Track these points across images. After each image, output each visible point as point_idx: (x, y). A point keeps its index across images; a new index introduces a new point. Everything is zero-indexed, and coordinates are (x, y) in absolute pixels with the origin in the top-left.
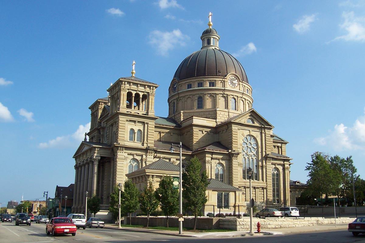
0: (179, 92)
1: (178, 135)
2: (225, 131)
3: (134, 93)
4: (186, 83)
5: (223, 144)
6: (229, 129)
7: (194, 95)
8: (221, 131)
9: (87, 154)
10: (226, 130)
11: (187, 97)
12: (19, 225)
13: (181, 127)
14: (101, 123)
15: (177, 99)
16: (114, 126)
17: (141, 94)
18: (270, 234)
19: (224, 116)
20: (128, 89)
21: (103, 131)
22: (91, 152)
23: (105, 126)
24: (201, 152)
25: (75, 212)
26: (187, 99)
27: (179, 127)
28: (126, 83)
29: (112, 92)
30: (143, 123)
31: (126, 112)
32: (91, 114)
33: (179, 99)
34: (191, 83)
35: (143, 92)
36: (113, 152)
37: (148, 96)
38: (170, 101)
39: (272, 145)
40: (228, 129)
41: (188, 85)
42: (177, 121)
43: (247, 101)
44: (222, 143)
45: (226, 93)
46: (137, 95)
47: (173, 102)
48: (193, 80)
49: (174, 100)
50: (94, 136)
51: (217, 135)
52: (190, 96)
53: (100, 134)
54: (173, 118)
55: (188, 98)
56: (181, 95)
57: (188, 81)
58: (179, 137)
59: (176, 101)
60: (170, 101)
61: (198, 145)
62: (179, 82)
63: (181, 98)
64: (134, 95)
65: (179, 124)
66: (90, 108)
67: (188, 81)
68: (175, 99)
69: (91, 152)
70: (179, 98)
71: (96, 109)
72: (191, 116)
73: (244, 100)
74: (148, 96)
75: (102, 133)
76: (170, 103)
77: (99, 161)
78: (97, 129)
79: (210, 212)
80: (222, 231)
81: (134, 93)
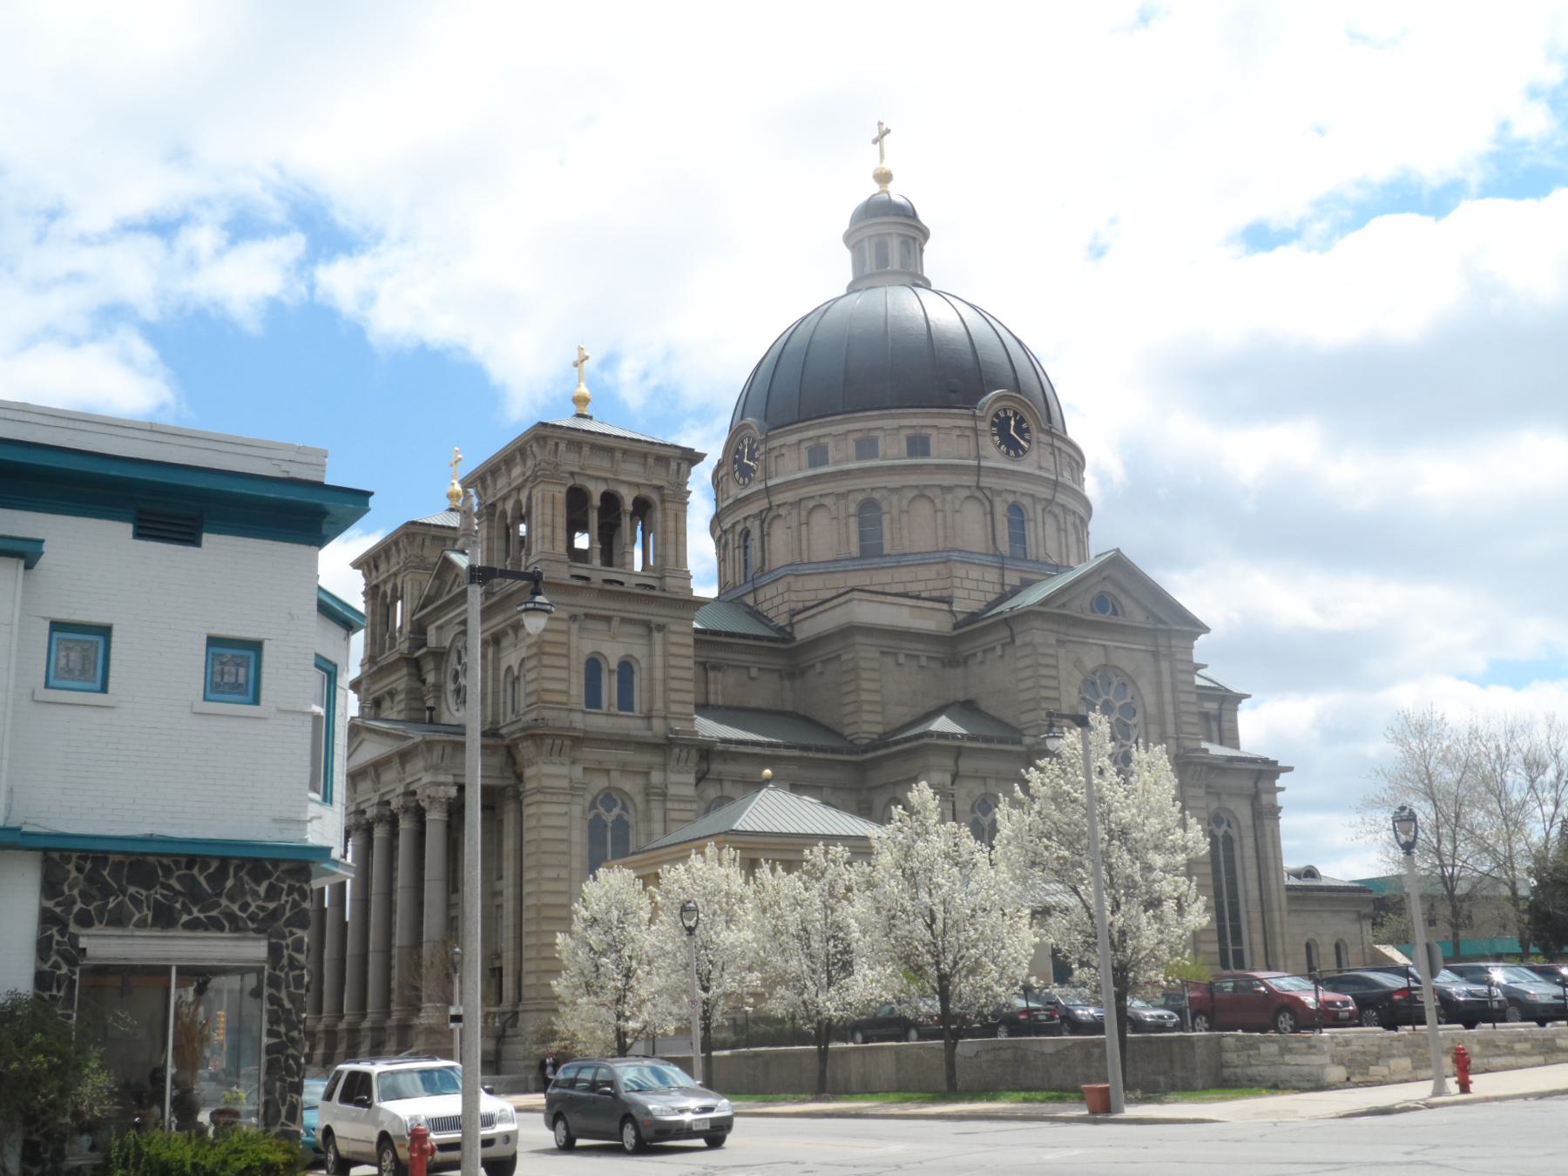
0: (771, 483)
1: (781, 677)
2: (999, 651)
3: (596, 491)
4: (901, 427)
5: (991, 712)
6: (1018, 642)
7: (949, 489)
8: (980, 655)
9: (378, 776)
10: (1003, 645)
11: (811, 504)
12: (580, 1142)
13: (793, 639)
14: (425, 633)
15: (761, 517)
16: (505, 643)
17: (628, 497)
18: (1025, 1100)
19: (983, 586)
20: (572, 474)
21: (438, 668)
22: (408, 767)
23: (447, 644)
24: (907, 752)
25: (365, 1047)
26: (810, 513)
27: (784, 640)
28: (562, 447)
29: (484, 488)
30: (649, 628)
31: (567, 576)
32: (365, 594)
33: (771, 515)
34: (928, 431)
35: (637, 485)
36: (514, 763)
37: (658, 503)
38: (726, 525)
39: (1193, 709)
40: (1013, 641)
41: (812, 451)
42: (771, 614)
43: (1070, 519)
44: (983, 705)
45: (987, 481)
46: (610, 500)
47: (739, 528)
48: (833, 429)
49: (745, 519)
50: (392, 694)
51: (960, 671)
52: (826, 501)
53: (424, 682)
54: (750, 600)
55: (816, 507)
56: (778, 499)
57: (811, 434)
58: (787, 684)
59: (757, 523)
60: (726, 525)
61: (879, 719)
62: (767, 439)
63: (782, 511)
64: (596, 500)
65: (781, 629)
66: (357, 565)
67: (917, 420)
68: (754, 516)
69: (403, 768)
70: (770, 509)
71: (394, 570)
72: (834, 593)
73: (1057, 510)
74: (658, 503)
75: (431, 678)
76: (725, 532)
77: (449, 805)
78: (406, 659)
79: (1393, 1033)
80: (790, 1096)
81: (596, 491)
